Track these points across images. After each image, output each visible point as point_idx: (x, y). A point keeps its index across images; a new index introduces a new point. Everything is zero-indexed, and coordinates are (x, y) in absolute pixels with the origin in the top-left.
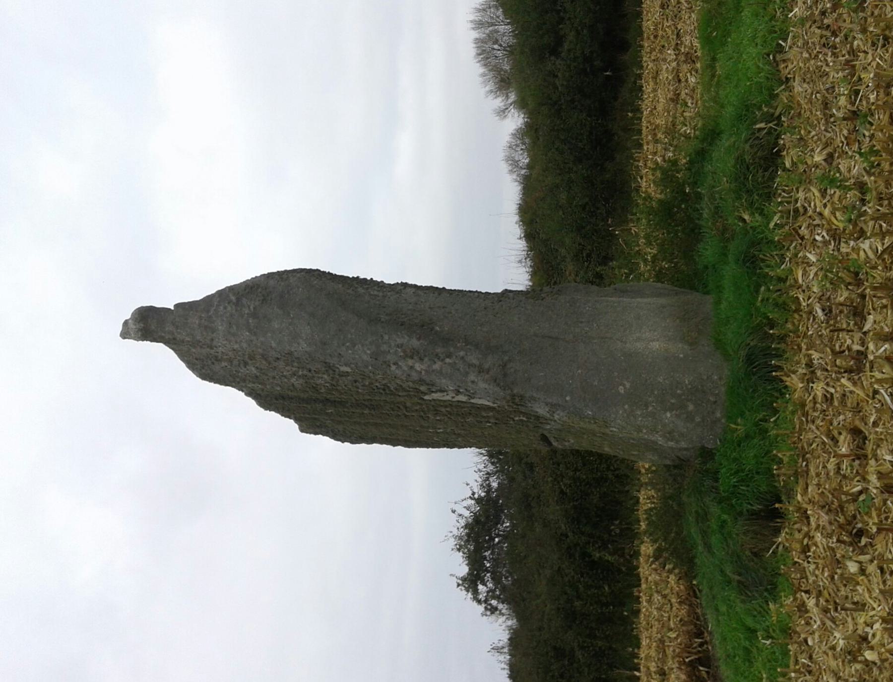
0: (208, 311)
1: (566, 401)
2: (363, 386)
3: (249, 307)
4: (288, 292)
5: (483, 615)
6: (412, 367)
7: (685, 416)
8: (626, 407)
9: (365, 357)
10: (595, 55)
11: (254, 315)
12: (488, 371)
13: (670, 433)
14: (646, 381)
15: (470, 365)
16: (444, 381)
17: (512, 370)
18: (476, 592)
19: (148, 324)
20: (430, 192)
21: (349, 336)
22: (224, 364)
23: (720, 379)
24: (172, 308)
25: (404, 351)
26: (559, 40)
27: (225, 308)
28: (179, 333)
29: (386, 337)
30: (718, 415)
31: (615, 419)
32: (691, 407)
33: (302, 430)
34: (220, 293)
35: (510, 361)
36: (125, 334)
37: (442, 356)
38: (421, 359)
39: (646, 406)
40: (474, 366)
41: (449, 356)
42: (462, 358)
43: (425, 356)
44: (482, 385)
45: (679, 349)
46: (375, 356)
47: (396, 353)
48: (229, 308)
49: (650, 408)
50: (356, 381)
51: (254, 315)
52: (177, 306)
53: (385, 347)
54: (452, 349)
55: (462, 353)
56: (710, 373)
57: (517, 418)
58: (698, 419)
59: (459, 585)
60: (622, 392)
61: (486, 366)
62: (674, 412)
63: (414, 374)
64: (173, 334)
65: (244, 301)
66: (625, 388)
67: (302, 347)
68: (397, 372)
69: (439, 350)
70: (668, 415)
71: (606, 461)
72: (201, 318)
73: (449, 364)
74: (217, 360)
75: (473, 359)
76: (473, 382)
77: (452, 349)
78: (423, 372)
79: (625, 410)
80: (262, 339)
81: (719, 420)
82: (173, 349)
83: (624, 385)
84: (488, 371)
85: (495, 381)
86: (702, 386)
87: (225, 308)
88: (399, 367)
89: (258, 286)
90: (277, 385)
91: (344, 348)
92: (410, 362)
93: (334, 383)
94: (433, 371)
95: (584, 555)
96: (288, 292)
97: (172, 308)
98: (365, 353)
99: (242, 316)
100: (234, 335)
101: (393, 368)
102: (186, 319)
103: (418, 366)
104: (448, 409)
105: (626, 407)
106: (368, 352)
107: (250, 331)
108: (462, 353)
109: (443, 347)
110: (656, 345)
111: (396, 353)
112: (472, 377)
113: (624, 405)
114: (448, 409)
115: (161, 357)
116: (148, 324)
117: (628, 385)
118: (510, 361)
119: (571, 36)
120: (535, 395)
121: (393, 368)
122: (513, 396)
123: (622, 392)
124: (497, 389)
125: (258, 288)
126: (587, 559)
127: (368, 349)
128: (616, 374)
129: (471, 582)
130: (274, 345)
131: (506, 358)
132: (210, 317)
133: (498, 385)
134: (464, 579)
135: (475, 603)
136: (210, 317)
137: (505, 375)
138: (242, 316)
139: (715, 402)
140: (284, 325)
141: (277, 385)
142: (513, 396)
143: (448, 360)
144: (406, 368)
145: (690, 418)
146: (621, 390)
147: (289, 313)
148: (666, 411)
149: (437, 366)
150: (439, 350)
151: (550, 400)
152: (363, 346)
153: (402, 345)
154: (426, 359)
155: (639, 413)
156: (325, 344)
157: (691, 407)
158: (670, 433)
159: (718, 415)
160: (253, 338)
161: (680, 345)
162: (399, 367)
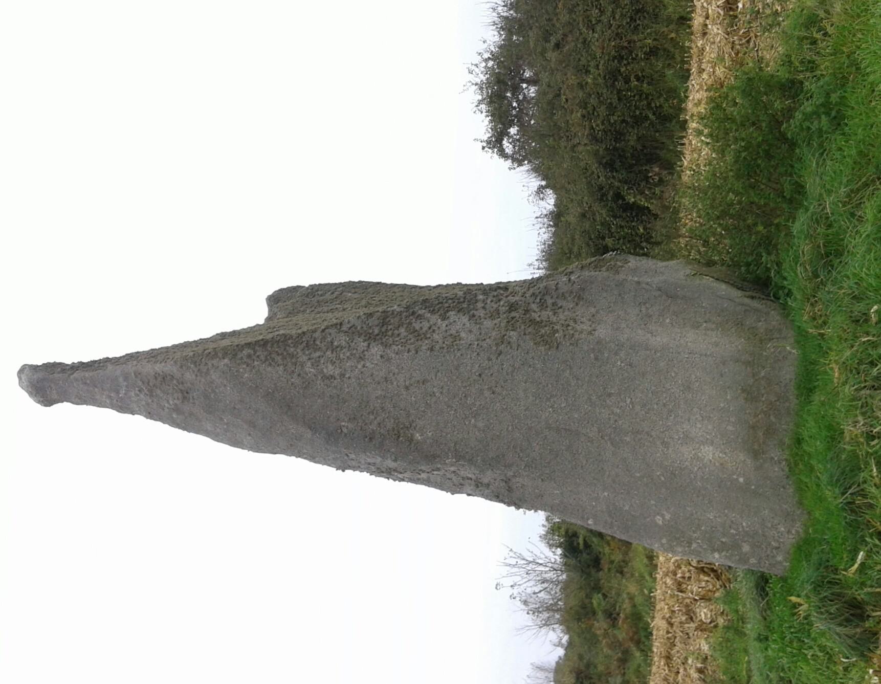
5: (510, 169)
7: (737, 557)
8: (664, 541)
12: (488, 485)
14: (692, 515)
18: (502, 154)
32: (746, 548)
45: (739, 463)
49: (694, 545)
59: (483, 148)
60: (660, 523)
61: (486, 481)
62: (723, 554)
71: (647, 98)
83: (663, 516)
95: (618, 196)
96: (214, 391)
105: (664, 541)
110: (708, 453)
113: (661, 538)
117: (668, 517)
118: (514, 476)
123: (660, 523)
126: (620, 202)
128: (653, 502)
129: (495, 143)
134: (489, 142)
135: (502, 160)
139: (777, 548)
146: (659, 520)
147: (221, 419)
148: (714, 551)
157: (746, 548)
161: (742, 457)
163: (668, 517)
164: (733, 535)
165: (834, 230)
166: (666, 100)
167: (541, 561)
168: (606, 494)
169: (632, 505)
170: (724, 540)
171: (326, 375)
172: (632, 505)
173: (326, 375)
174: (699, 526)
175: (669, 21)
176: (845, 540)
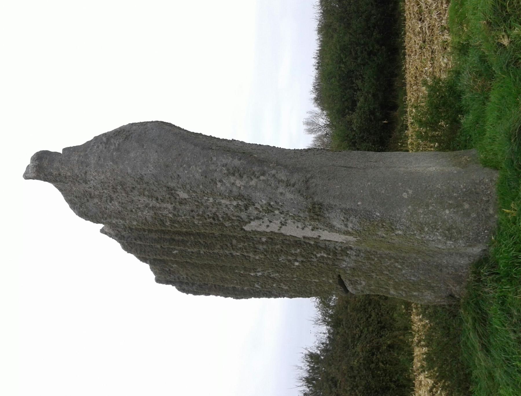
0: (86, 151)
1: (358, 205)
2: (198, 215)
3: (115, 144)
4: (145, 132)
6: (233, 184)
9: (197, 176)
10: (376, 110)
11: (118, 150)
13: (449, 230)
15: (280, 181)
16: (258, 194)
17: (314, 185)
19: (44, 166)
20: (257, 83)
21: (186, 159)
22: (96, 200)
23: (491, 181)
24: (61, 152)
25: (228, 170)
26: (354, 103)
27: (98, 147)
28: (63, 169)
29: (215, 159)
30: (491, 212)
31: (400, 218)
33: (159, 280)
34: (96, 138)
35: (312, 177)
36: (26, 177)
37: (257, 174)
38: (241, 177)
39: (427, 206)
40: (282, 181)
41: (263, 174)
42: (274, 175)
43: (244, 173)
44: (289, 196)
46: (205, 174)
47: (221, 171)
48: (101, 147)
49: (431, 208)
50: (192, 211)
51: (118, 150)
52: (64, 150)
53: (213, 167)
54: (266, 168)
55: (274, 172)
56: (482, 178)
57: (318, 255)
58: (474, 215)
60: (406, 197)
61: (292, 181)
62: (451, 210)
63: (235, 189)
64: (59, 170)
65: (112, 140)
66: (408, 194)
67: (149, 171)
68: (222, 188)
69: (255, 169)
70: (447, 212)
72: (80, 156)
73: (264, 180)
74: (91, 197)
75: (282, 175)
76: (281, 194)
77: (266, 168)
78: (242, 188)
79: (409, 210)
80: (121, 167)
81: (492, 216)
82: (60, 190)
83: (407, 192)
84: (294, 185)
85: (299, 192)
86: (475, 189)
87: (98, 147)
88: (223, 184)
89: (124, 130)
90: (134, 219)
91: (181, 169)
92: (232, 179)
93: (176, 213)
94: (250, 186)
96: (145, 132)
97: (61, 152)
98: (198, 172)
99: (109, 151)
100: (102, 166)
101: (219, 185)
102: (69, 158)
103: (238, 183)
104: (265, 247)
105: (410, 207)
106: (200, 171)
107: (113, 161)
108: (274, 172)
109: (259, 166)
111: (221, 171)
112: (281, 190)
114: (265, 247)
115: (49, 193)
116: (44, 166)
117: (410, 192)
118: (312, 177)
119: (362, 99)
120: (332, 202)
121: (219, 185)
122: (314, 204)
123: (406, 197)
124: (301, 199)
125: (124, 131)
127: (200, 169)
130: (129, 171)
131: (309, 175)
132: (87, 155)
133: (302, 195)
136: (87, 155)
137: (308, 188)
138: (109, 151)
140: (138, 154)
141: (134, 219)
142: (314, 204)
143: (262, 178)
144: (228, 185)
145: (467, 214)
147: (143, 146)
148: (444, 210)
149: (253, 183)
150: (255, 169)
151: (344, 206)
152: (196, 166)
153: (226, 165)
154: (245, 176)
155: (421, 211)
156: (167, 166)
157: (466, 206)
158: (449, 230)
159: (491, 212)
160: (115, 167)
162: (223, 184)
163: (410, 192)
164: (456, 198)
165: (179, 207)
166: (401, 375)
167: (343, 169)
168: (369, 183)
169: (386, 189)
170: (451, 202)
171: (171, 205)
172: (386, 189)
173: (171, 205)
174: (432, 195)
175: (399, 329)
176: (340, 26)
